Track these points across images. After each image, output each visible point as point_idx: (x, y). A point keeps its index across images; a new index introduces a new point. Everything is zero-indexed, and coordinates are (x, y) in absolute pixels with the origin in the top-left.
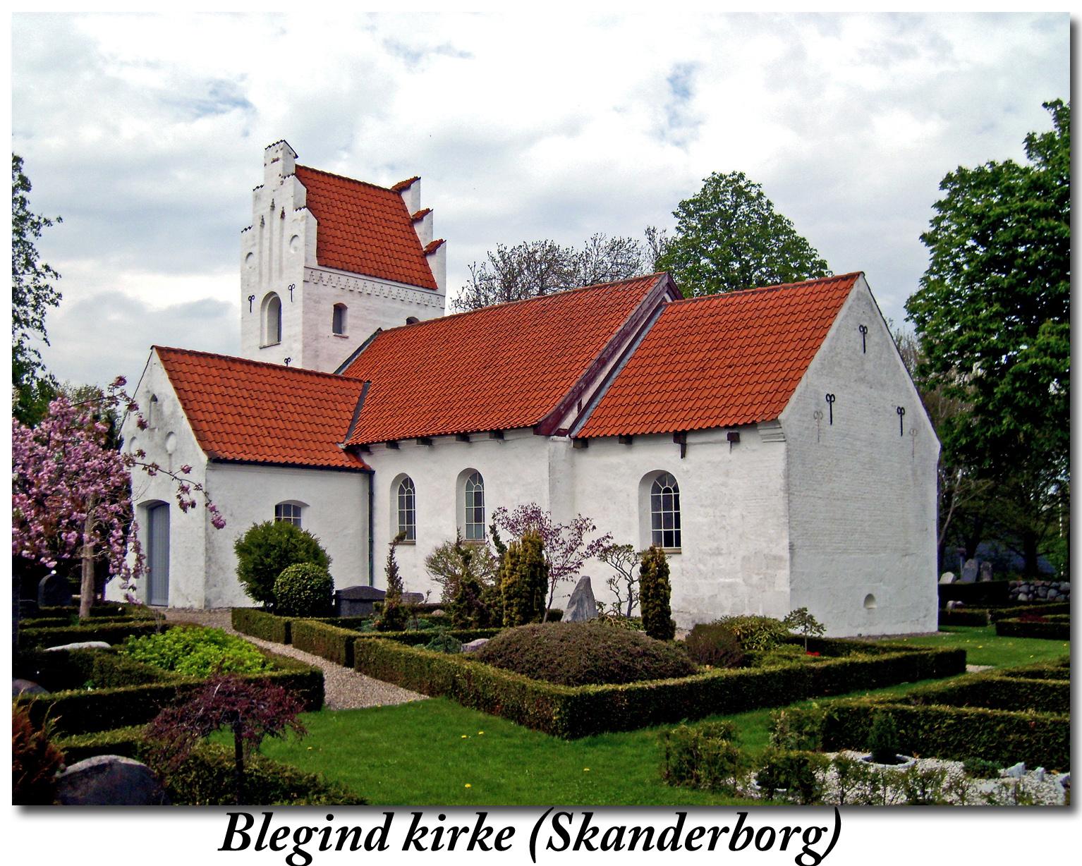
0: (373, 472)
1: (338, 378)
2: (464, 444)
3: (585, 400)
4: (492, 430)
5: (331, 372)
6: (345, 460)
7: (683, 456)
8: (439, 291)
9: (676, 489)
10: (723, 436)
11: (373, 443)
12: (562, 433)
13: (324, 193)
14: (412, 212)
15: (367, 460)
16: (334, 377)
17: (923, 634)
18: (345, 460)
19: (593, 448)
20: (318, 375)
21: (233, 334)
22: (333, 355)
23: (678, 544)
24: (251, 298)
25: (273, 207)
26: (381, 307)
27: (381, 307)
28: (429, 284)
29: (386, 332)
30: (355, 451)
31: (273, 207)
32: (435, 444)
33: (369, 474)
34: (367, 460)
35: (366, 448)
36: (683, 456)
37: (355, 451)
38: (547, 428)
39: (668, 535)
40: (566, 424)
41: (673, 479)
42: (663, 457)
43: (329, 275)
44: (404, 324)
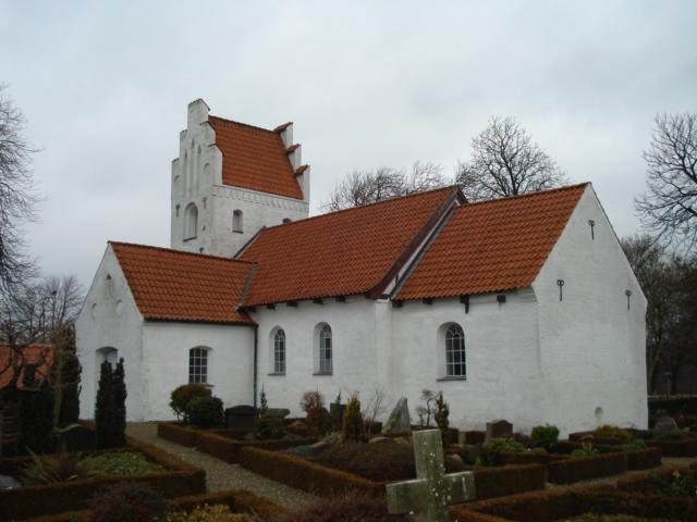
2: (318, 306)
6: (235, 317)
12: (385, 297)
14: (288, 146)
19: (406, 307)
24: (178, 207)
26: (265, 210)
27: (265, 210)
33: (255, 327)
35: (253, 309)
38: (373, 294)
40: (388, 291)
42: (453, 313)
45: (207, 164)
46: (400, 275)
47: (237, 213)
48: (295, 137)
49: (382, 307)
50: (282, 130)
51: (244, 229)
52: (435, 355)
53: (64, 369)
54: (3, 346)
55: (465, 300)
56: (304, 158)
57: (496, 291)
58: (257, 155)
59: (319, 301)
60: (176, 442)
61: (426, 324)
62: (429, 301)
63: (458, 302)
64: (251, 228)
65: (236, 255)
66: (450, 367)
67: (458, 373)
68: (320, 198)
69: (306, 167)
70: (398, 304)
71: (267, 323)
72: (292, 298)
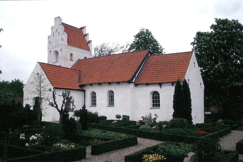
0: (85, 91)
1: (72, 69)
2: (91, 86)
3: (136, 76)
4: (98, 83)
5: (70, 68)
6: (79, 88)
7: (161, 88)
8: (91, 51)
9: (96, 95)
10: (171, 84)
11: (94, 83)
12: (133, 83)
13: (68, 28)
14: (84, 34)
15: (84, 88)
16: (71, 69)
17: (77, 111)
18: (79, 88)
19: (139, 86)
20: (67, 68)
21: (46, 61)
22: (69, 65)
23: (96, 105)
24: (50, 51)
25: (56, 31)
26: (79, 54)
27: (79, 54)
28: (88, 49)
29: (81, 60)
30: (82, 86)
31: (56, 31)
32: (120, 83)
33: (84, 91)
34: (84, 88)
35: (84, 85)
36: (161, 88)
37: (82, 86)
38: (130, 82)
39: (94, 103)
40: (133, 81)
41: (159, 94)
42: (156, 88)
43: (69, 47)
44: (84, 58)
45: (50, 41)
46: (136, 76)
47: (71, 54)
48: (87, 31)
49: (132, 85)
50: (82, 28)
51: (73, 60)
52: (149, 100)
53: (179, 118)
54: (241, 37)
55: (160, 84)
56: (90, 38)
57: (172, 82)
58: (76, 36)
59: (110, 83)
60: (125, 147)
61: (145, 92)
62: (147, 84)
63: (158, 85)
64: (76, 58)
65: (72, 68)
66: (92, 103)
67: (94, 104)
68: (93, 53)
69: (91, 41)
70: (136, 85)
71: (89, 91)
72: (129, 79)
